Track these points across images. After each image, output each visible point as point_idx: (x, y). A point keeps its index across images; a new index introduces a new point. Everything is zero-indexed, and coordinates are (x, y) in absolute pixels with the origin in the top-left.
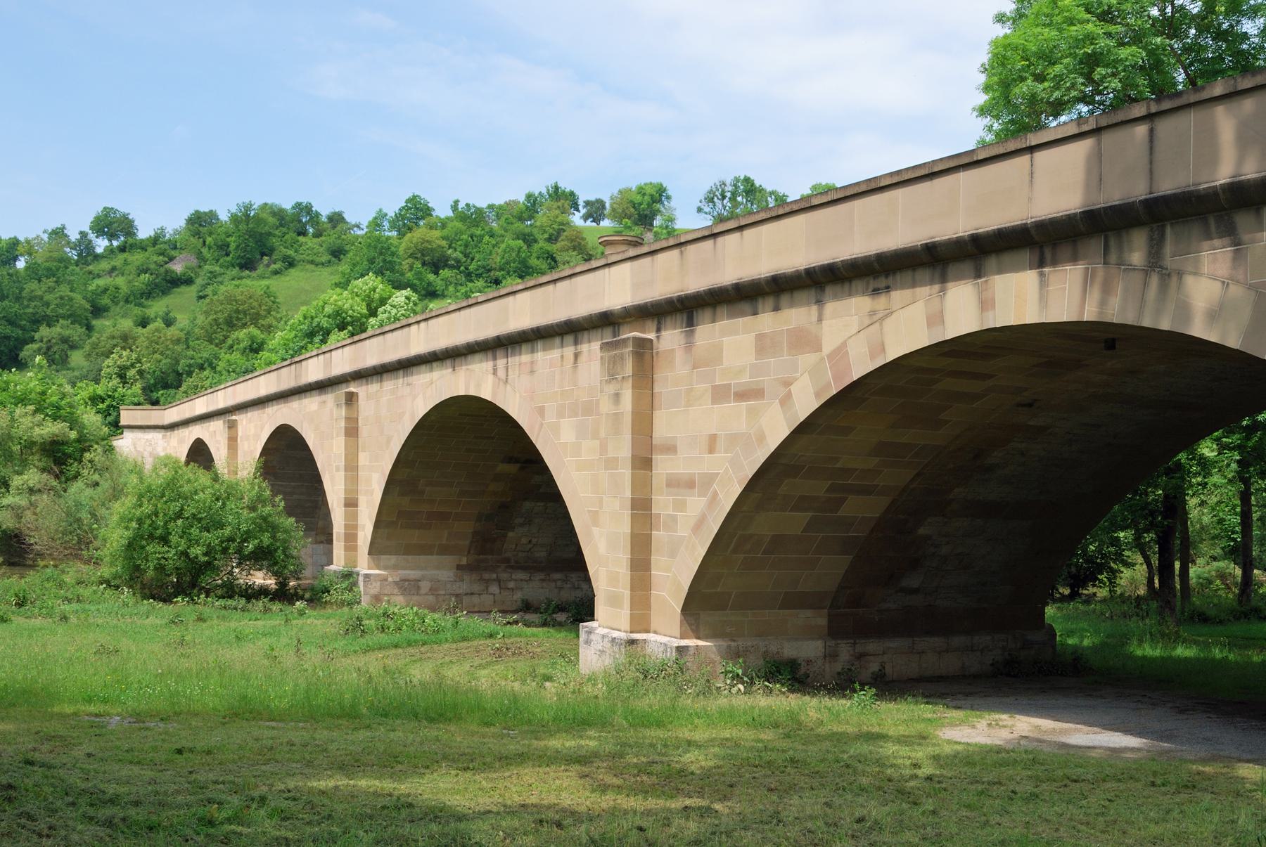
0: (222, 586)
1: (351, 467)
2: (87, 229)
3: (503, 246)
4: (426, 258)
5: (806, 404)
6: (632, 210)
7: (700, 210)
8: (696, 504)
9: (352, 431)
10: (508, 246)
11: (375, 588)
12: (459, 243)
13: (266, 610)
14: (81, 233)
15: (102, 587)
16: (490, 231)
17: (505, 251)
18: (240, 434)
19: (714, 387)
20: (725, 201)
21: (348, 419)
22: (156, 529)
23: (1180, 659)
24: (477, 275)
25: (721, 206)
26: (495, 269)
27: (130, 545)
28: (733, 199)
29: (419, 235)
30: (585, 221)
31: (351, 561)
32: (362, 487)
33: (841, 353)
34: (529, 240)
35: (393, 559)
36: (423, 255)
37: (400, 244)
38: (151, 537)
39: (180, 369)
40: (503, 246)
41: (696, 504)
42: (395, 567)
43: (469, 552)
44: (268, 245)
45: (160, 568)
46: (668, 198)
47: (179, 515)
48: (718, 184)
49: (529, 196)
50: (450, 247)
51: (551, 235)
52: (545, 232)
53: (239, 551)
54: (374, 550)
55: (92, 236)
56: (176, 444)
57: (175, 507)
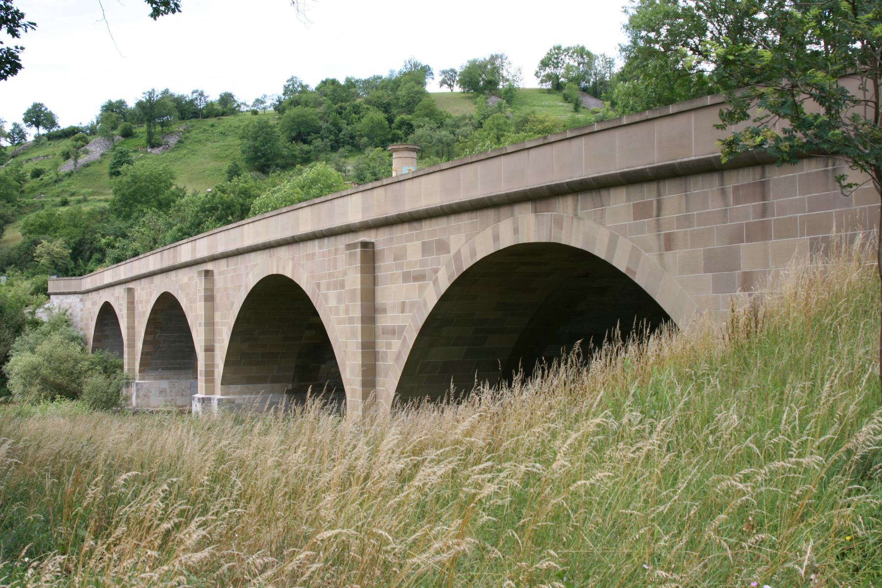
1: (210, 324)
2: (20, 121)
5: (444, 284)
8: (396, 343)
14: (15, 124)
18: (136, 299)
19: (403, 273)
21: (206, 290)
32: (217, 338)
33: (458, 255)
35: (239, 387)
41: (396, 343)
42: (241, 393)
43: (293, 380)
54: (225, 381)
55: (23, 126)
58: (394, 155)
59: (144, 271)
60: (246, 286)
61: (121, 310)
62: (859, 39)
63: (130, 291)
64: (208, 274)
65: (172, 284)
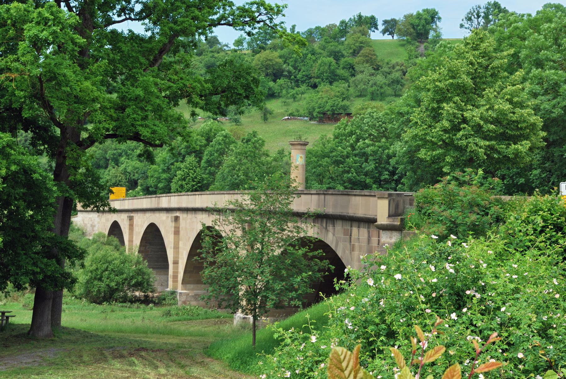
0: (122, 298)
1: (176, 248)
3: (319, 62)
4: (268, 71)
6: (412, 30)
7: (462, 26)
10: (322, 62)
11: (184, 298)
12: (291, 60)
13: (138, 307)
16: (312, 51)
17: (320, 65)
18: (135, 223)
20: (480, 19)
21: (175, 227)
22: (97, 275)
24: (302, 82)
25: (476, 23)
26: (314, 77)
27: (88, 282)
28: (486, 17)
29: (264, 56)
30: (384, 34)
31: (175, 287)
32: (180, 256)
34: (337, 56)
36: (267, 69)
37: (253, 60)
38: (95, 278)
39: (107, 157)
40: (319, 62)
42: (193, 290)
45: (99, 291)
46: (439, 18)
47: (106, 270)
48: (475, 8)
49: (343, 22)
50: (285, 62)
51: (354, 50)
52: (350, 48)
53: (129, 283)
54: (184, 282)
56: (104, 221)
57: (105, 266)
61: (125, 228)
64: (177, 219)
65: (157, 219)
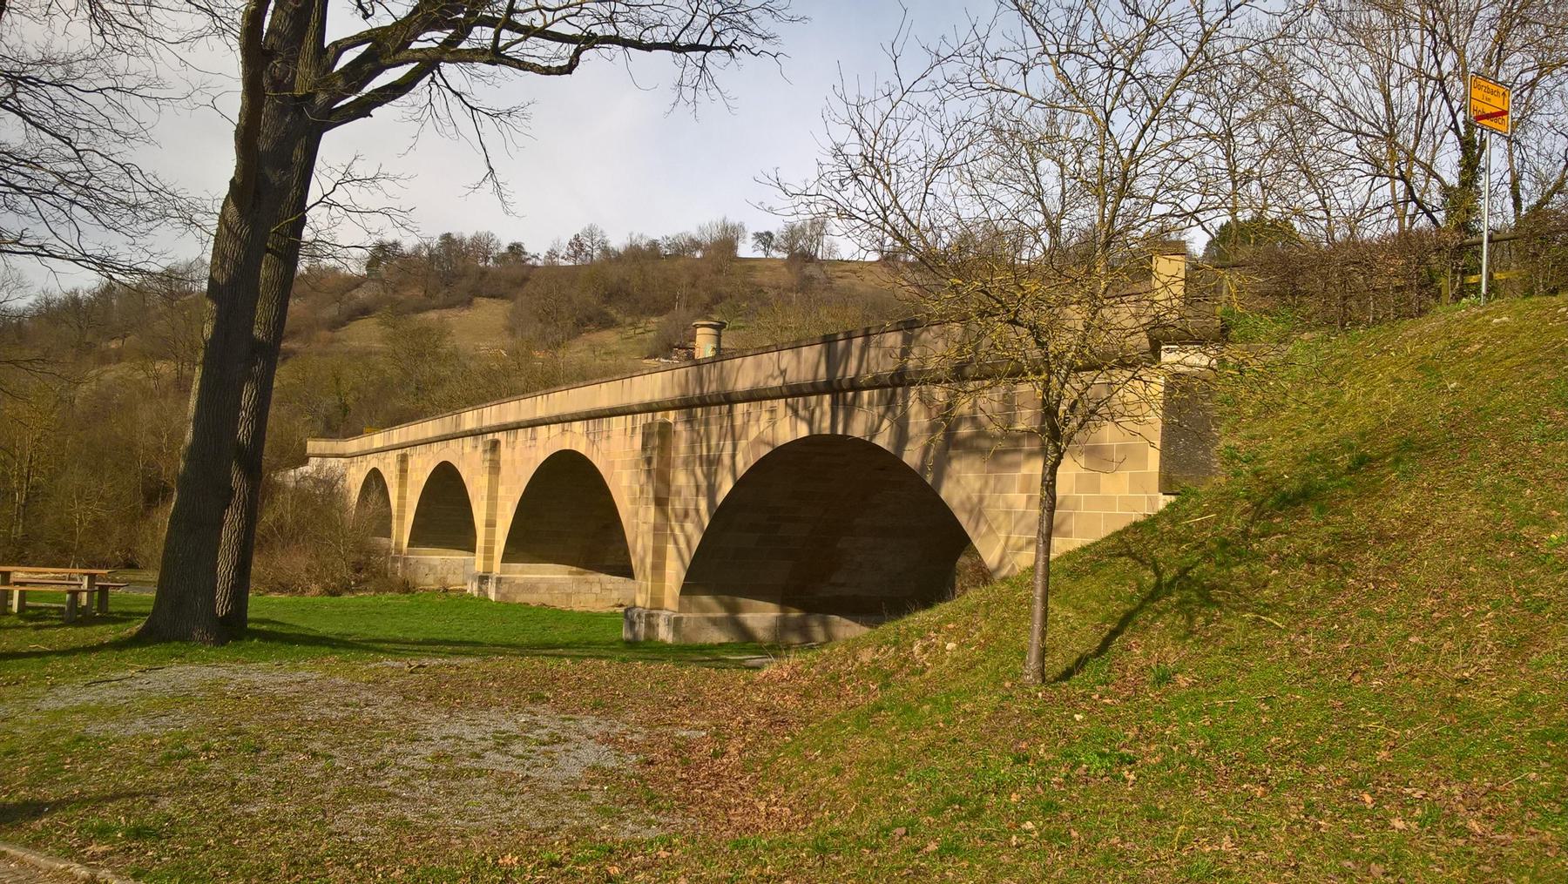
1: (492, 498)
9: (495, 468)
15: (1366, 167)
23: (245, 128)
32: (499, 512)
44: (356, 269)
58: (699, 331)
59: (421, 436)
60: (536, 462)
62: (1341, 245)
63: (403, 460)
